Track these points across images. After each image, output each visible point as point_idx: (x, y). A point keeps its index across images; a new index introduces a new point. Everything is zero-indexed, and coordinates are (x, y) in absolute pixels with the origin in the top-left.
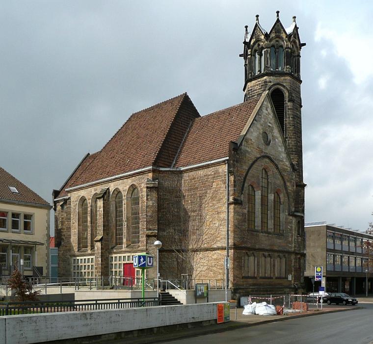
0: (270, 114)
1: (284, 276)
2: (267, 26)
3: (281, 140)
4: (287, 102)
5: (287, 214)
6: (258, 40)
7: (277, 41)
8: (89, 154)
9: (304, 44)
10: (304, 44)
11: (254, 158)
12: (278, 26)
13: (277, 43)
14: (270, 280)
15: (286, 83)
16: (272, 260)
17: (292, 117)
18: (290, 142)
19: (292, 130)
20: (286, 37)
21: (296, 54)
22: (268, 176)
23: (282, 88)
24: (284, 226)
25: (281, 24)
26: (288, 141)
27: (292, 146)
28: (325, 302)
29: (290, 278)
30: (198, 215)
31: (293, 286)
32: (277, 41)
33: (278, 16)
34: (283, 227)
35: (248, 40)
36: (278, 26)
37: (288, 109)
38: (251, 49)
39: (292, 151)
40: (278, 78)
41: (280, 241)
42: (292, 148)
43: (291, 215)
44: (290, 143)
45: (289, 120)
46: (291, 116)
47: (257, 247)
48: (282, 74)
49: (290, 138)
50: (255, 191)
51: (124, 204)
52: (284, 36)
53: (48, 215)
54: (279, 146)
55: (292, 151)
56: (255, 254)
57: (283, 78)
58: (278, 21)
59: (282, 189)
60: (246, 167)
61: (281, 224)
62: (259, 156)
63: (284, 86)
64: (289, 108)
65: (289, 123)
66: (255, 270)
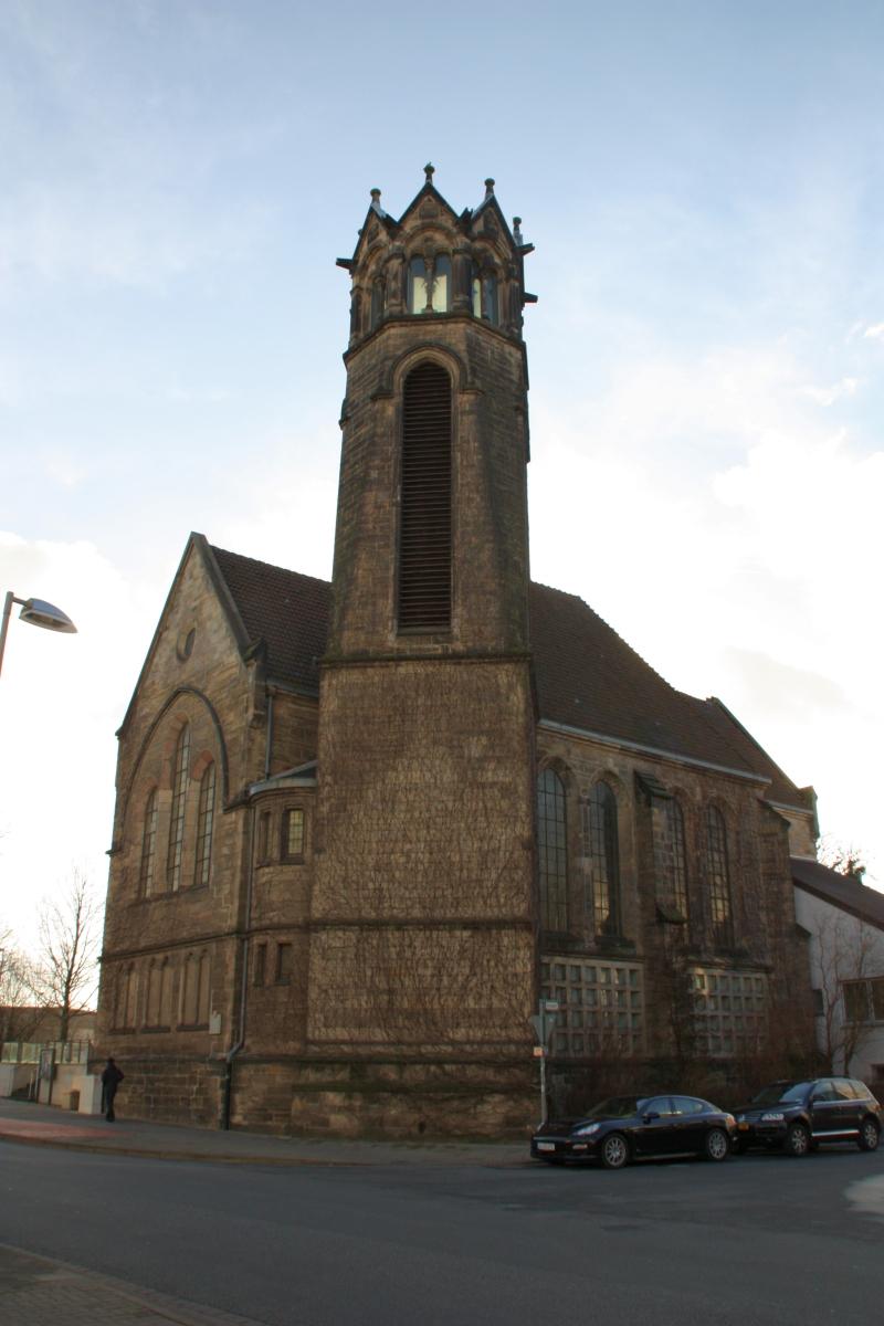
58: (429, 190)
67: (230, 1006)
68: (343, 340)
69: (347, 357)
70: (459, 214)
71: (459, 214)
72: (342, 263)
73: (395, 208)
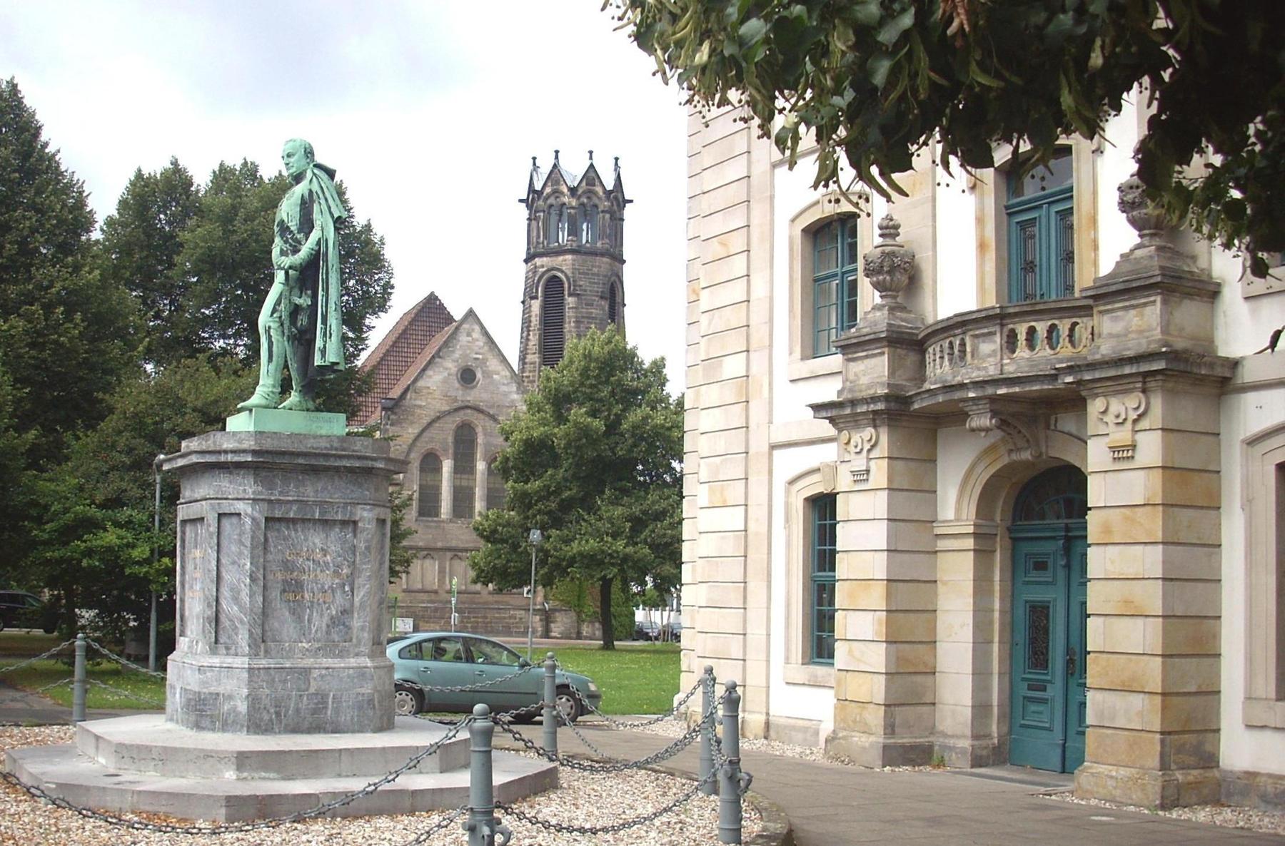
2: (574, 171)
6: (556, 193)
8: (791, 168)
9: (631, 201)
10: (631, 201)
11: (433, 415)
12: (591, 175)
21: (618, 215)
23: (559, 274)
28: (555, 717)
30: (588, 378)
33: (591, 158)
35: (538, 186)
36: (591, 175)
38: (533, 199)
47: (439, 545)
48: (561, 251)
57: (561, 258)
60: (412, 431)
62: (447, 408)
63: (562, 271)
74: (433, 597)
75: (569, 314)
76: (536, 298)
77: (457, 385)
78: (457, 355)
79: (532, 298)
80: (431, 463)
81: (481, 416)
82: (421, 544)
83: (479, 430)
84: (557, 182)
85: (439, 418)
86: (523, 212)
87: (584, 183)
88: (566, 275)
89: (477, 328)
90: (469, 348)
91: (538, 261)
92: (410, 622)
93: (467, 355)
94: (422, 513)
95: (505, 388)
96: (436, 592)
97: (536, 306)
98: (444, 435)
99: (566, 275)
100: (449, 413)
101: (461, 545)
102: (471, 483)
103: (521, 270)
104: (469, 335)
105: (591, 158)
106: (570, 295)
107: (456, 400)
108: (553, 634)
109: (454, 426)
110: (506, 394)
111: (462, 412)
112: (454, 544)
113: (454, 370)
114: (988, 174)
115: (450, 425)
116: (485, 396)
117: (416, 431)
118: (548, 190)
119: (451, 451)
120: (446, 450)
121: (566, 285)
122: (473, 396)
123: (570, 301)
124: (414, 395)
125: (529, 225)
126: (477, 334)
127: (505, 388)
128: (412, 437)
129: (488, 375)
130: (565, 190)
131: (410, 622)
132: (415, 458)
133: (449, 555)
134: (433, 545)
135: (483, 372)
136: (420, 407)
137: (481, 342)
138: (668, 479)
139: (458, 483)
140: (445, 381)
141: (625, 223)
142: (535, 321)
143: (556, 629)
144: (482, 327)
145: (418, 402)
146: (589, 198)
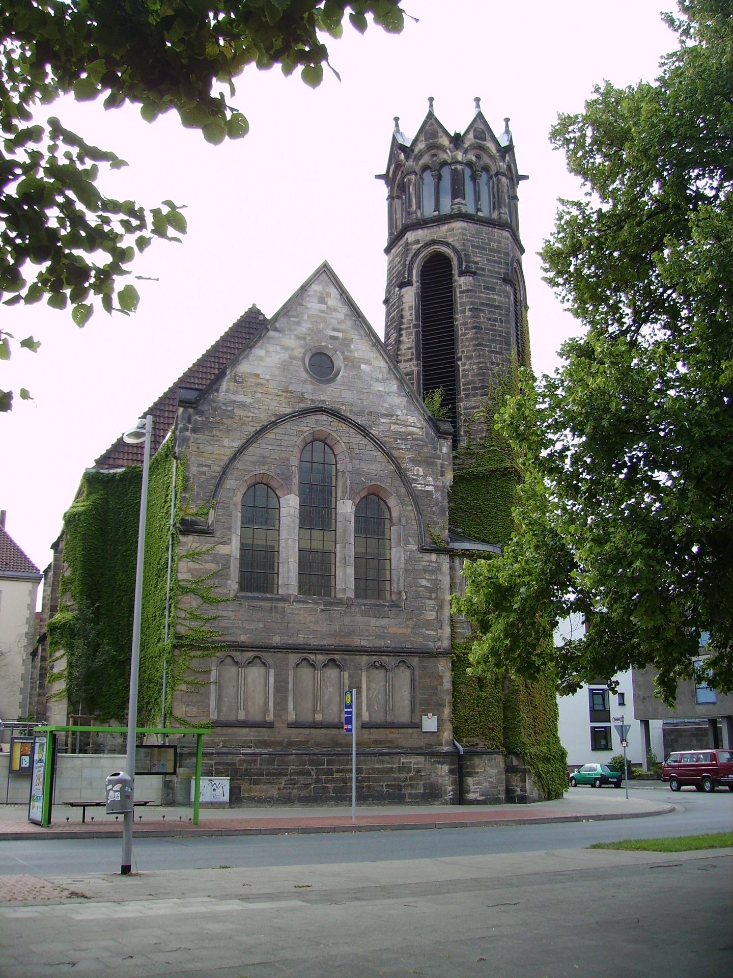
0: (335, 310)
1: (405, 718)
3: (383, 364)
4: (456, 277)
5: (415, 548)
7: (435, 155)
10: (526, 177)
11: (265, 418)
13: (435, 159)
14: (334, 732)
15: (454, 235)
16: (346, 674)
17: (470, 310)
18: (467, 367)
19: (472, 339)
20: (451, 143)
22: (335, 456)
23: (443, 249)
24: (402, 580)
25: (436, 120)
26: (465, 365)
27: (473, 376)
29: (430, 723)
31: (446, 749)
32: (435, 155)
33: (478, 106)
34: (398, 583)
37: (461, 292)
39: (475, 388)
40: (435, 229)
41: (384, 622)
42: (472, 382)
43: (431, 551)
44: (469, 370)
45: (465, 317)
46: (467, 308)
47: (276, 640)
49: (469, 358)
50: (278, 498)
51: (345, 564)
52: (445, 141)
53: (33, 594)
54: (377, 380)
55: (475, 388)
56: (270, 661)
57: (445, 228)
58: (431, 115)
59: (389, 484)
61: (394, 577)
62: (288, 410)
63: (447, 244)
64: (464, 288)
65: (465, 324)
66: (266, 703)
67: (447, 711)
68: (383, 240)
69: (387, 251)
70: (452, 135)
71: (452, 135)
72: (378, 177)
73: (409, 134)
74: (265, 734)
75: (461, 299)
76: (409, 283)
77: (304, 375)
78: (303, 329)
79: (402, 285)
80: (260, 511)
81: (344, 427)
82: (243, 638)
83: (340, 448)
84: (434, 135)
85: (274, 424)
86: (383, 190)
87: (471, 136)
88: (454, 249)
89: (334, 292)
90: (324, 321)
91: (410, 236)
92: (224, 783)
93: (320, 331)
94: (245, 584)
95: (380, 387)
96: (270, 726)
97: (410, 295)
98: (285, 448)
99: (454, 249)
100: (292, 416)
101: (314, 642)
102: (329, 546)
103: (384, 260)
104: (322, 300)
105: (478, 106)
106: (462, 273)
107: (302, 399)
108: (471, 796)
109: (299, 441)
110: (380, 395)
111: (312, 419)
112: (300, 639)
113: (299, 352)
114: (597, 550)
115: (292, 437)
116: (348, 396)
117: (237, 444)
118: (421, 146)
119: (296, 481)
120: (287, 479)
121: (455, 263)
122: (329, 394)
123: (462, 282)
124: (232, 386)
125: (390, 206)
126: (334, 299)
127: (380, 387)
128: (230, 452)
129: (352, 363)
130: (445, 141)
131: (224, 783)
132: (235, 491)
133: (293, 658)
134: (267, 642)
135: (345, 359)
136: (243, 405)
137: (342, 311)
138: (661, 477)
139: (306, 545)
140: (285, 367)
141: (519, 203)
142: (409, 316)
143: (475, 787)
144: (343, 292)
145: (240, 398)
146: (478, 157)
